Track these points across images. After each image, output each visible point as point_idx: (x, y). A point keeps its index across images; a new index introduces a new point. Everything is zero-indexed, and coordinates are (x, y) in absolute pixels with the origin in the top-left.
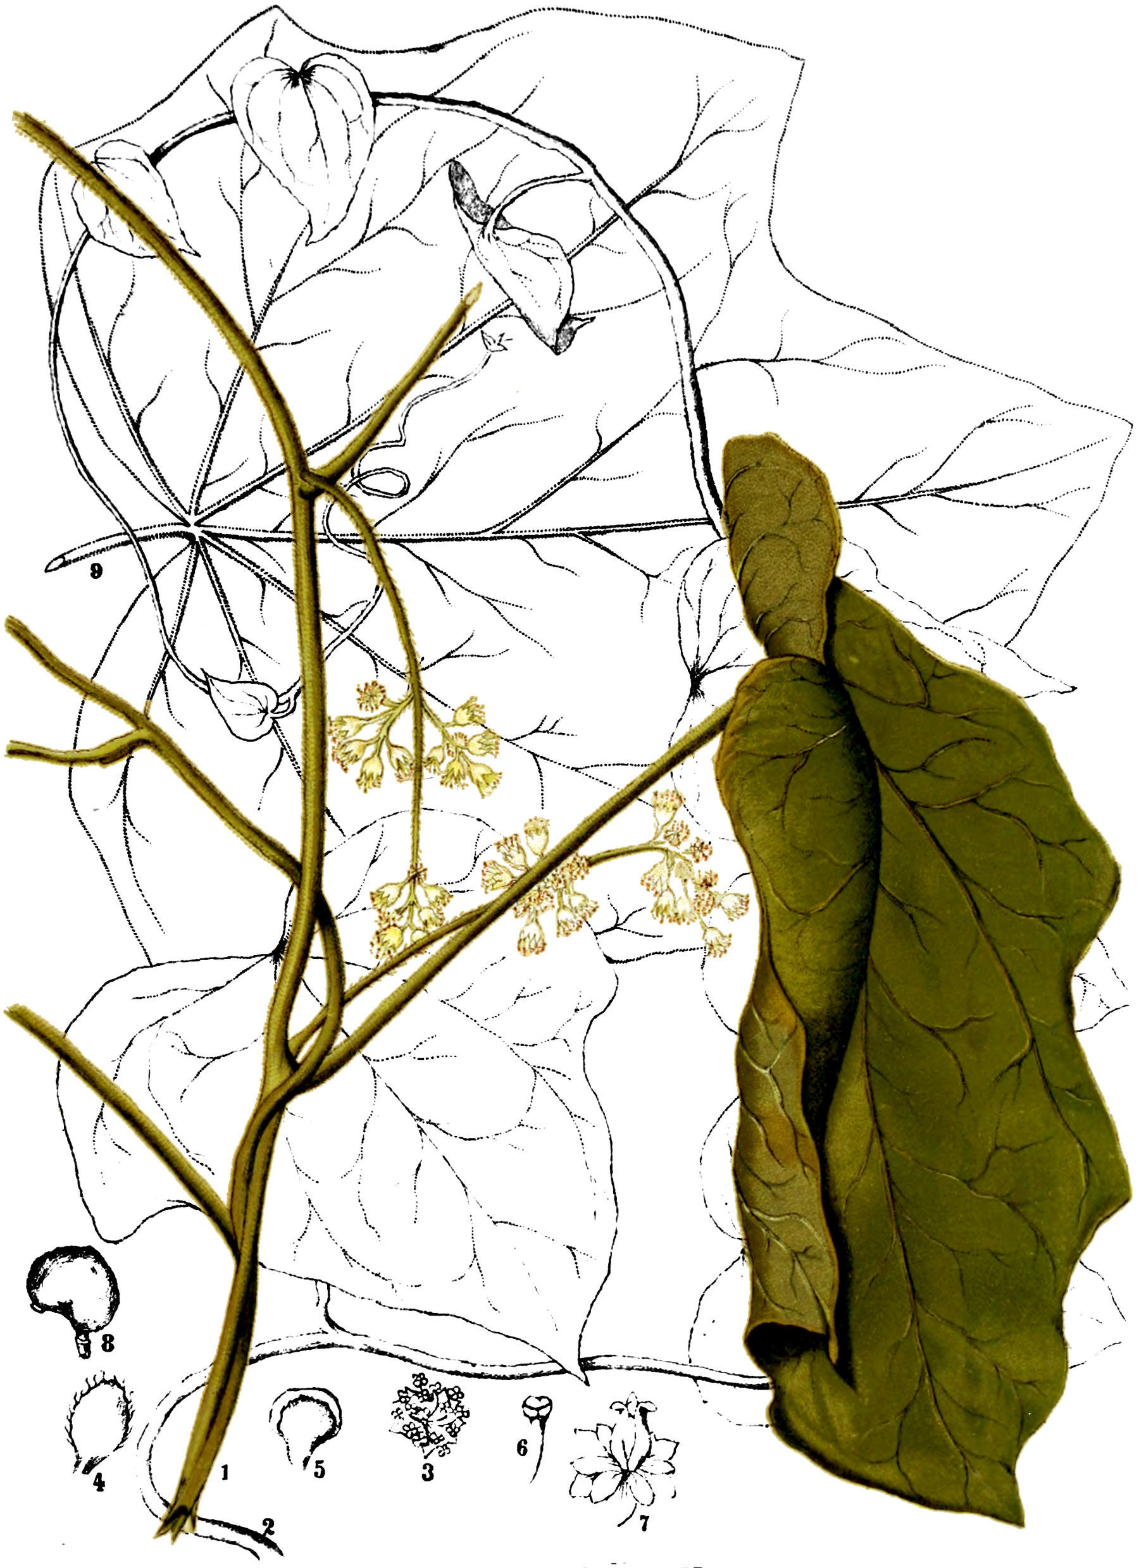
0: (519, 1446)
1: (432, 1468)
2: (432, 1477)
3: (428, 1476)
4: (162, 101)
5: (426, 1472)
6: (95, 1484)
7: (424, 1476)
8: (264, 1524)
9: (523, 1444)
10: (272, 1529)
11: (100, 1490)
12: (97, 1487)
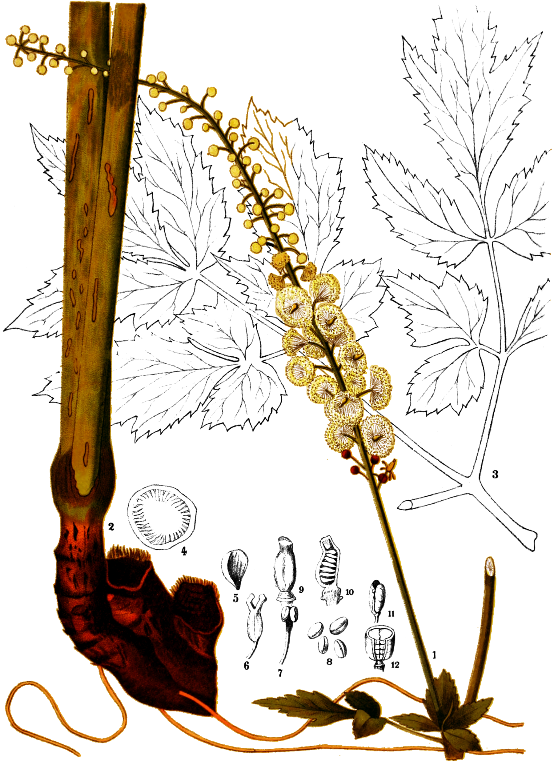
0: (245, 665)
1: (497, 472)
2: (497, 476)
3: (495, 476)
4: (522, 544)
6: (182, 552)
7: (493, 476)
8: (109, 525)
9: (247, 664)
11: (184, 555)
12: (183, 554)
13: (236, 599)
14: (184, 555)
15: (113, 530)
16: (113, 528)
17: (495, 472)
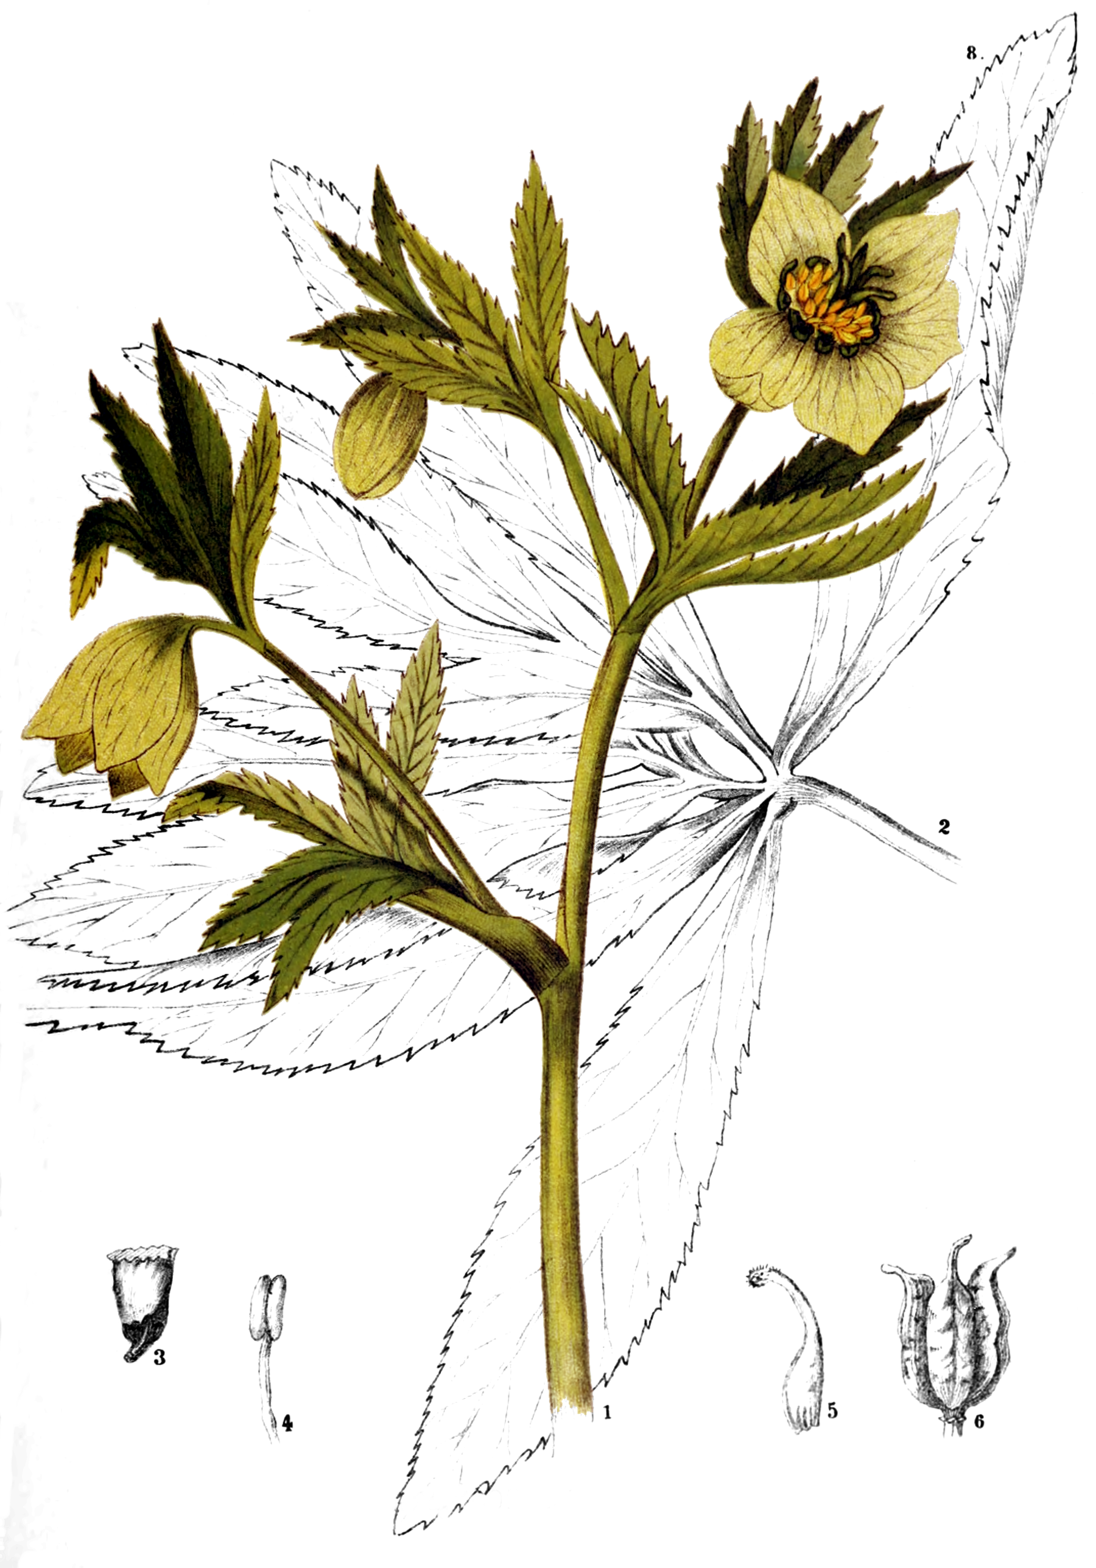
1: (163, 1353)
2: (163, 1361)
3: (160, 1362)
5: (158, 1357)
6: (284, 1425)
7: (156, 1362)
10: (947, 830)
11: (288, 1430)
12: (285, 1428)
13: (832, 1412)
14: (288, 1430)
15: (946, 833)
16: (947, 830)
17: (159, 1352)
